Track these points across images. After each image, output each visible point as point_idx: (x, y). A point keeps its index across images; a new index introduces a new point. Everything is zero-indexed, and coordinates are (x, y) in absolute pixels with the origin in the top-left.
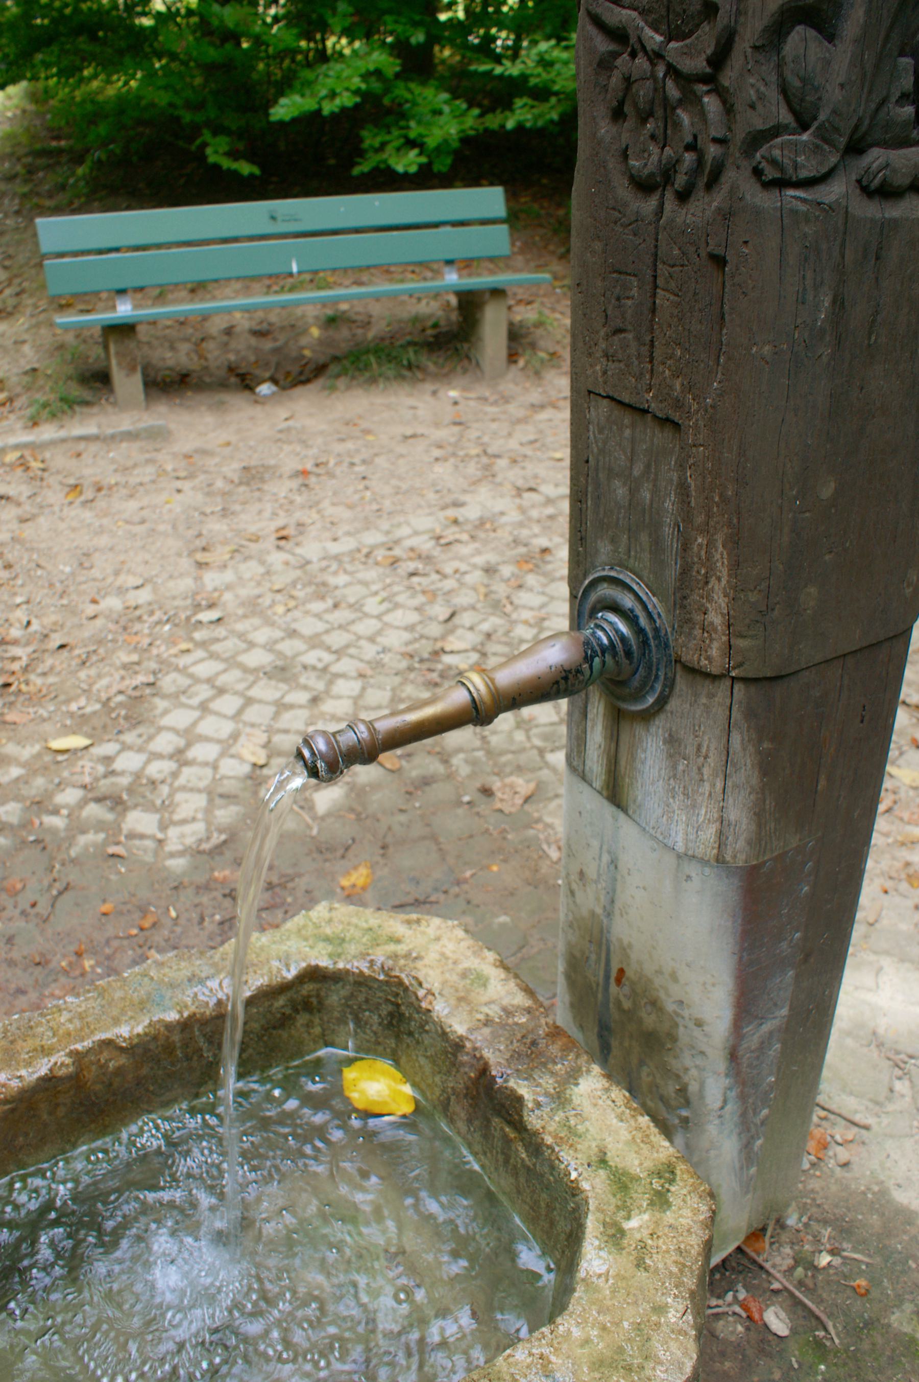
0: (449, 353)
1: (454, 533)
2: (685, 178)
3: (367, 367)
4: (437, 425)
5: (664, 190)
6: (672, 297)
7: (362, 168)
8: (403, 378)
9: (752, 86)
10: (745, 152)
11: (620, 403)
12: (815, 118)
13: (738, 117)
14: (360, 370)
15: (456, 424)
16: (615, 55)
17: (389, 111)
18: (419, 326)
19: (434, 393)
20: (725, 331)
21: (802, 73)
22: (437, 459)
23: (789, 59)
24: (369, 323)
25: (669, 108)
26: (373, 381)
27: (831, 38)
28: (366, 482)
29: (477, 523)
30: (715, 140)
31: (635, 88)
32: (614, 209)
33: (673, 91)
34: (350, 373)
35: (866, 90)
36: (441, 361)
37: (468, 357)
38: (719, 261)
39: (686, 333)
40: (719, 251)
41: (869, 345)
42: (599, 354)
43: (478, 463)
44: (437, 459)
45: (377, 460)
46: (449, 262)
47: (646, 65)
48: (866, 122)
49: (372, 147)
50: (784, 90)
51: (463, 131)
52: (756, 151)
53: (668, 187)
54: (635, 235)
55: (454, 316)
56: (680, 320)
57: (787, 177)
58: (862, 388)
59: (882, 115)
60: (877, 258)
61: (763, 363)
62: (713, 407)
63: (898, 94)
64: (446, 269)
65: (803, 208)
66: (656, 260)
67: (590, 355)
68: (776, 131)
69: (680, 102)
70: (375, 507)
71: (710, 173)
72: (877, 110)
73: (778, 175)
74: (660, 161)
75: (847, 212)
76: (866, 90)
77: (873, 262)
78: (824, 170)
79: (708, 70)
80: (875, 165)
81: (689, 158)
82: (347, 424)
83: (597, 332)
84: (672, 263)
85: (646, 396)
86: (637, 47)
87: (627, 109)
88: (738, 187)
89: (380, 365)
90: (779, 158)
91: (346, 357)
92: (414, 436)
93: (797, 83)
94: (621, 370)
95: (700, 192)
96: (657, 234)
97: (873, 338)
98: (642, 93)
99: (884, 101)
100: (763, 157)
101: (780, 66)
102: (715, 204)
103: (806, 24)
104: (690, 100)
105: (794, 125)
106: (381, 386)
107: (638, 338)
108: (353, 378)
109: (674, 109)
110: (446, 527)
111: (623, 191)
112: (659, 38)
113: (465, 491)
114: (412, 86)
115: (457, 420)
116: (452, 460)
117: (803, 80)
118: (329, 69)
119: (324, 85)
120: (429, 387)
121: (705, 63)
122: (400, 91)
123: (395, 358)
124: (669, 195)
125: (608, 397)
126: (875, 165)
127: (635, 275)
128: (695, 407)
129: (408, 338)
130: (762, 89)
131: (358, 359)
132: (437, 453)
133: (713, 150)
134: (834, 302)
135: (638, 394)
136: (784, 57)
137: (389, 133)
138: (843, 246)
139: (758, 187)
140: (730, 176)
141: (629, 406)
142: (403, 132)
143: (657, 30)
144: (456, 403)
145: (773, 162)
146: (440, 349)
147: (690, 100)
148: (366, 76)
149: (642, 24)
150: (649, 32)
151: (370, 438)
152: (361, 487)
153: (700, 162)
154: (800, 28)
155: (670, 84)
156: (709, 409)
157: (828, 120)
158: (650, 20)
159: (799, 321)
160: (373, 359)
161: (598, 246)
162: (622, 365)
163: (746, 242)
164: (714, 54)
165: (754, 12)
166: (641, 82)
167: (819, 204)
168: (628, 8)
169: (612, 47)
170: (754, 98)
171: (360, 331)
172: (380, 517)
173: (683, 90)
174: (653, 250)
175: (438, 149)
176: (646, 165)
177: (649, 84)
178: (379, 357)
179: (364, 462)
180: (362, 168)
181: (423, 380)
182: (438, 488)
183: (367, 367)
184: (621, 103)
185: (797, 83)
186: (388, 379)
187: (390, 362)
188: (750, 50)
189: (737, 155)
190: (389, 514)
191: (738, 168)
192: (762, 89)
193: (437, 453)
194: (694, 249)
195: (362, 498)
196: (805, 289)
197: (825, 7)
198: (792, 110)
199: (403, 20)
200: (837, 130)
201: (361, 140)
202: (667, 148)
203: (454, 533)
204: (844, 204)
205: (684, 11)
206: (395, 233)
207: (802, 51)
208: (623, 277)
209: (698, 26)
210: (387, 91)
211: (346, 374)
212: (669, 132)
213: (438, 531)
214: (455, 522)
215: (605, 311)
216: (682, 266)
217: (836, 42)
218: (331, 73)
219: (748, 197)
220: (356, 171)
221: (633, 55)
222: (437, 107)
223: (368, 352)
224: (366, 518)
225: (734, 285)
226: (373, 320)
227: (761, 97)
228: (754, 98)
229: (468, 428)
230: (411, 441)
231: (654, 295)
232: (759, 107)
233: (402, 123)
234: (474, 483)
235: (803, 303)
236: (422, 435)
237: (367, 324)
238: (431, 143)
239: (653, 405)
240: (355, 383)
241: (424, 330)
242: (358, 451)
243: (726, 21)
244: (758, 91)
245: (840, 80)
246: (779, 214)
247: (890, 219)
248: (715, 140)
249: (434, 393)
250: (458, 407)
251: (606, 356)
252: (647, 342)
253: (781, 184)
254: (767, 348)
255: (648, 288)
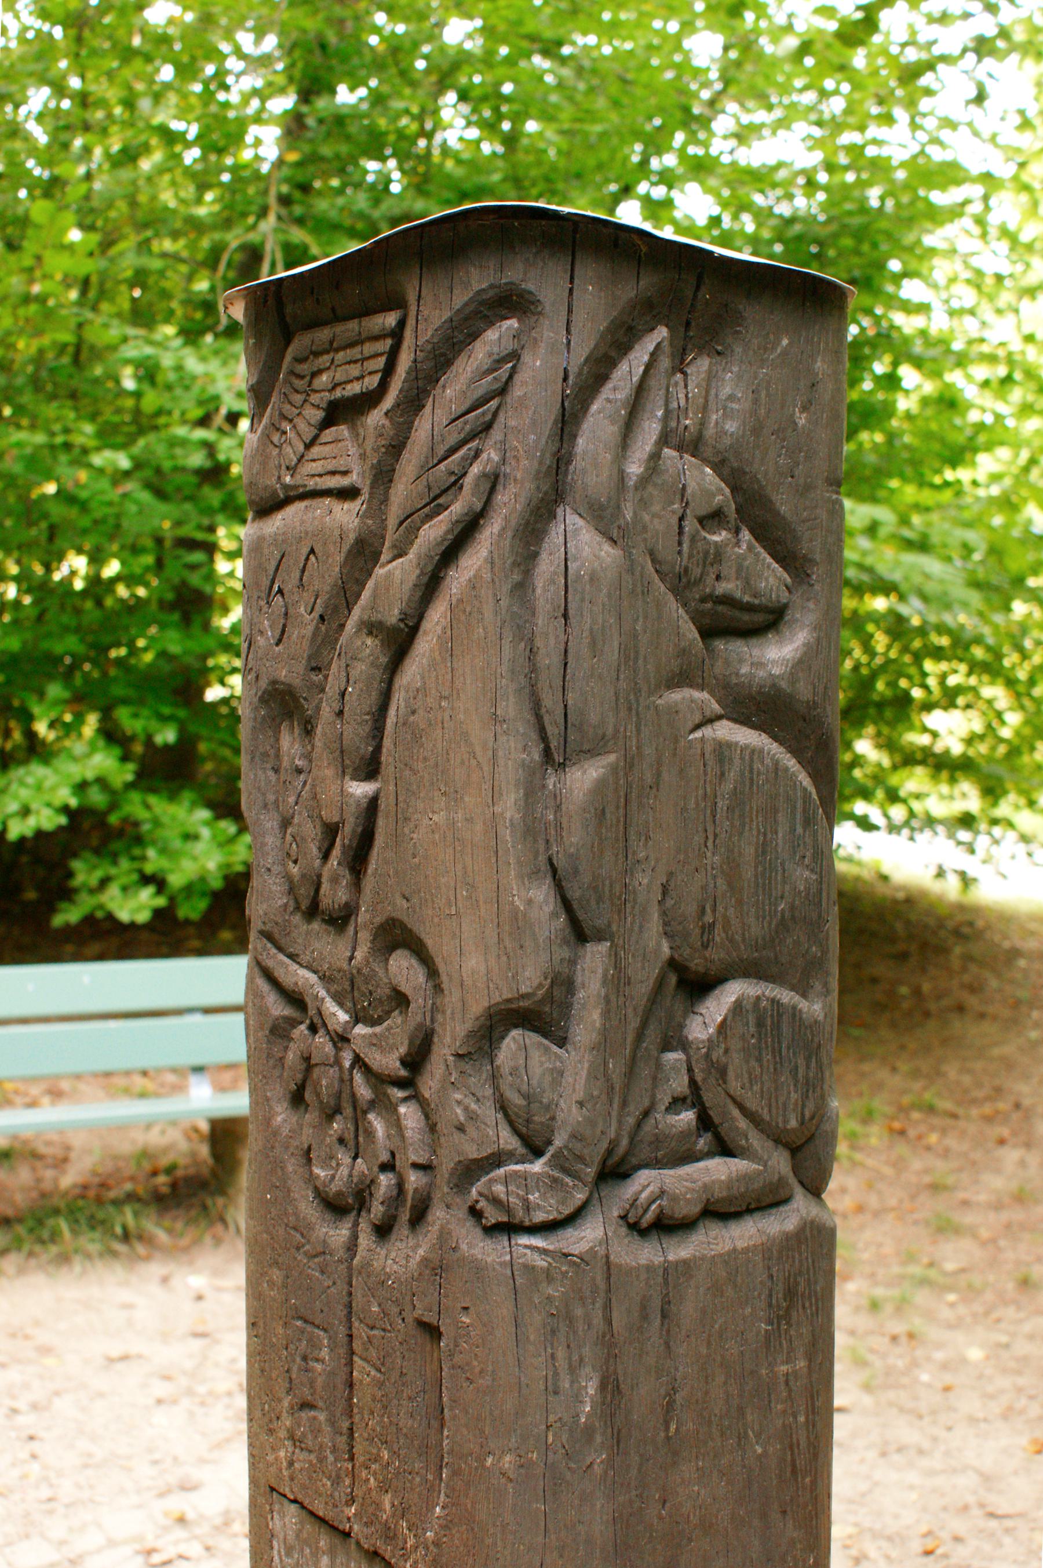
0: (193, 1213)
1: (176, 1543)
2: (381, 1208)
3: (55, 1237)
4: (165, 1337)
5: (359, 1215)
6: (373, 1373)
7: (69, 915)
8: (114, 1254)
9: (459, 1102)
10: (457, 1186)
11: (312, 1514)
12: (549, 1143)
13: (442, 1140)
14: (42, 1242)
15: (197, 1335)
16: (294, 1023)
17: (120, 833)
18: (147, 1166)
19: (165, 1280)
20: (446, 1433)
21: (524, 1088)
22: (160, 1402)
23: (505, 1070)
24: (65, 1160)
25: (359, 1114)
26: (64, 1259)
27: (562, 1042)
28: (35, 1446)
29: (218, 1521)
30: (415, 1166)
31: (316, 1072)
32: (295, 1228)
33: (364, 1091)
34: (26, 1247)
35: (615, 1106)
36: (179, 1225)
37: (223, 1220)
38: (433, 1332)
39: (394, 1429)
40: (430, 1318)
41: (668, 1438)
42: (283, 1434)
43: (228, 1407)
44: (160, 1402)
45: (58, 1403)
46: (198, 1069)
47: (329, 1048)
48: (625, 1142)
49: (84, 885)
50: (503, 1106)
51: (228, 865)
52: (472, 1184)
53: (363, 1214)
54: (322, 1272)
55: (204, 1151)
56: (385, 1407)
57: (516, 1221)
58: (665, 1502)
59: (648, 1126)
60: (664, 1316)
61: (503, 1480)
62: (437, 1544)
63: (667, 1100)
64: (193, 1080)
65: (541, 1262)
66: (350, 1313)
67: (271, 1431)
68: (497, 1160)
69: (372, 1104)
70: (45, 1493)
71: (413, 1207)
72: (639, 1125)
73: (505, 1219)
74: (350, 1175)
75: (608, 1263)
76: (615, 1106)
77: (657, 1322)
78: (567, 1211)
79: (403, 1073)
80: (644, 1195)
81: (385, 1180)
82: (13, 1336)
83: (280, 1400)
84: (370, 1322)
85: (346, 1510)
86: (317, 1020)
87: (308, 1095)
88: (449, 1233)
89: (75, 1232)
90: (503, 1197)
91: (20, 1220)
92: (125, 1358)
93: (520, 1101)
94: (310, 1462)
95: (402, 1229)
96: (350, 1277)
97: (673, 1427)
98: (324, 1082)
99: (646, 1114)
100: (481, 1194)
101: (495, 1077)
102: (421, 1252)
103: (524, 1027)
104: (382, 1104)
105: (521, 1150)
106: (77, 1268)
107: (332, 1422)
108: (31, 1254)
109: (365, 1113)
110: (166, 1529)
111: (308, 1208)
112: (343, 1017)
113: (202, 1461)
114: (153, 800)
115: (201, 1329)
116: (186, 1403)
117: (527, 1097)
118: (28, 773)
119: (16, 797)
120: (155, 1269)
121: (398, 1063)
122: (135, 806)
123: (103, 1222)
124: (364, 1226)
125: (294, 1501)
126: (644, 1195)
127: (325, 1330)
128: (411, 1542)
129: (128, 1186)
130: (473, 1106)
131: (40, 1222)
132: (161, 1389)
133: (414, 1179)
134: (603, 1387)
135: (335, 1506)
136: (498, 1067)
137: (115, 863)
138: (608, 1307)
139: (478, 1232)
140: (438, 1214)
141: (322, 1520)
142: (136, 865)
143: (341, 1005)
144: (200, 1298)
145: (495, 1201)
146: (178, 1205)
147: (382, 1104)
148: (81, 787)
149: (323, 993)
150: (331, 1006)
151: (50, 1361)
152: (24, 1455)
153: (400, 1186)
154: (515, 1033)
155: (358, 1077)
156: (432, 1547)
157: (566, 1147)
158: (332, 990)
159: (552, 1418)
160: (64, 1225)
161: (276, 1275)
162: (313, 1457)
163: (466, 1309)
164: (408, 1054)
165: (453, 1013)
166: (322, 1068)
167: (566, 1255)
168: (306, 967)
169: (288, 1011)
170: (462, 1119)
171: (49, 1174)
172: (51, 1512)
173: (375, 1089)
174: (346, 1299)
175: (189, 889)
176: (333, 1177)
177: (333, 1072)
178: (77, 1221)
179: (35, 1407)
180: (69, 915)
181: (147, 1258)
182: (157, 1456)
183: (55, 1237)
184: (301, 1088)
185: (518, 1100)
186: (88, 1256)
187: (93, 1228)
188: (452, 1058)
189: (446, 1189)
190: (67, 1506)
191: (448, 1207)
192: (473, 1106)
193: (161, 1389)
194: (397, 1310)
195: (24, 1477)
196: (556, 1374)
197: (547, 1009)
198: (516, 1132)
199: (145, 712)
200: (581, 1159)
201: (70, 874)
202: (359, 1160)
203: (176, 1543)
204: (602, 1252)
205: (371, 993)
206: (112, 1024)
207: (522, 1062)
208: (309, 1328)
209: (388, 1013)
210: (113, 806)
211: (19, 1249)
212: (361, 1139)
213: (150, 1542)
214: (181, 1520)
215: (288, 1371)
216: (384, 1330)
217: (569, 1047)
218: (30, 780)
219: (464, 1247)
220: (58, 920)
221: (313, 1029)
222: (191, 830)
223: (56, 1212)
224: (27, 1515)
225: (453, 1367)
226: (73, 1155)
227: (472, 1116)
228: (462, 1119)
229: (217, 1342)
230: (119, 1366)
231: (350, 1363)
232: (471, 1131)
233: (137, 851)
234: (218, 1446)
235: (556, 1393)
236: (140, 1356)
237: (62, 1162)
238: (176, 880)
239: (356, 1527)
240: (33, 1262)
241: (155, 1173)
242: (26, 1386)
243: (419, 1018)
244: (466, 1109)
245: (580, 1095)
246: (509, 1272)
247: (677, 1263)
248: (415, 1166)
249: (165, 1280)
250: (203, 1305)
251: (292, 1437)
252: (345, 1430)
253: (510, 1228)
254: (508, 1458)
255: (342, 1351)
